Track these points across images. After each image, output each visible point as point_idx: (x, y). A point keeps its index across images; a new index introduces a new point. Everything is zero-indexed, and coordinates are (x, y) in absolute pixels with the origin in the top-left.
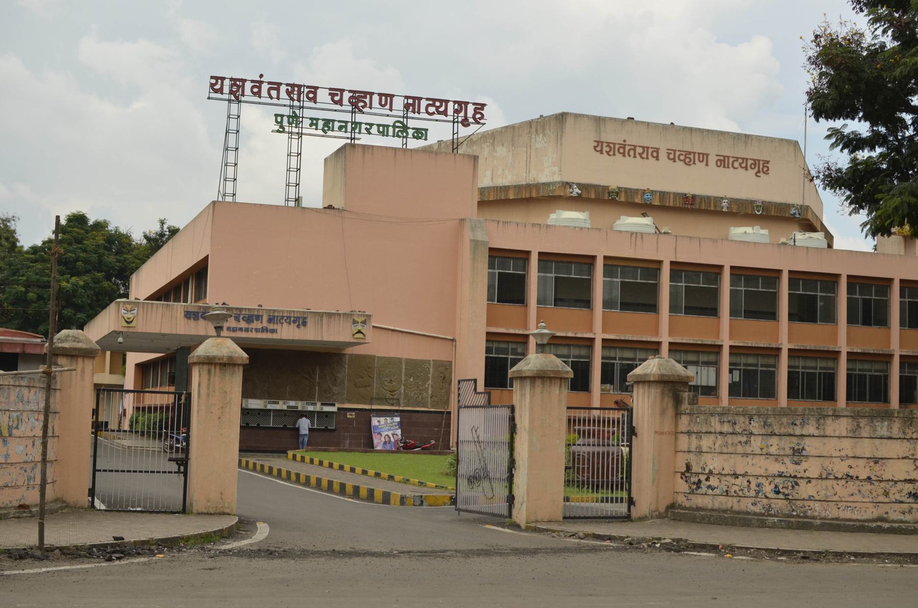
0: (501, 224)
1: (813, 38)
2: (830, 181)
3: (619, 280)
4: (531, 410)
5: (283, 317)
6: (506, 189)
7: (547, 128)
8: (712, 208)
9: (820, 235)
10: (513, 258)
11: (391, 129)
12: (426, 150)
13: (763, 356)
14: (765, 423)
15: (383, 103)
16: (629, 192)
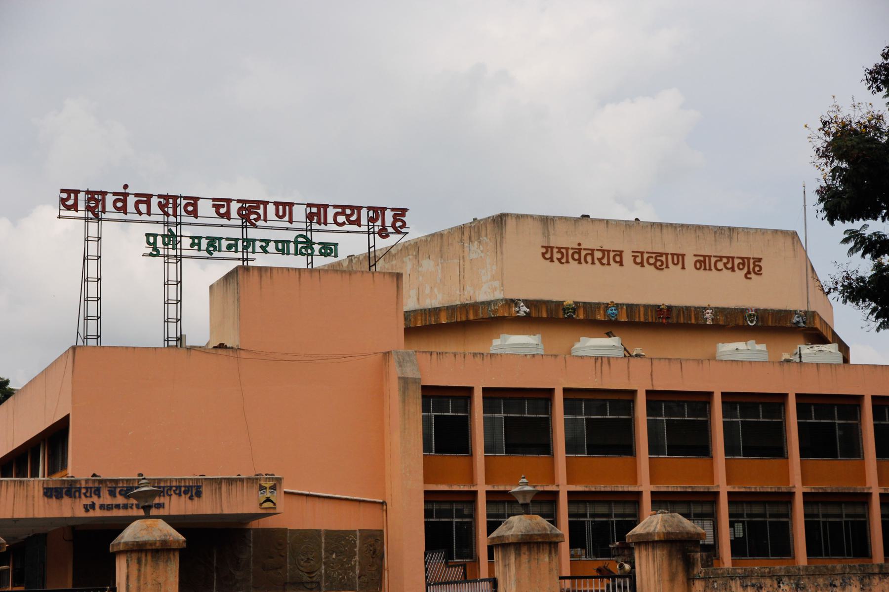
0: (434, 356)
1: (821, 126)
2: (851, 293)
3: (584, 417)
4: (518, 582)
5: (171, 487)
6: (436, 311)
7: (483, 233)
8: (693, 321)
9: (833, 348)
10: (452, 397)
11: (292, 246)
12: (334, 269)
13: (771, 503)
14: (797, 585)
15: (281, 214)
16: (588, 306)
